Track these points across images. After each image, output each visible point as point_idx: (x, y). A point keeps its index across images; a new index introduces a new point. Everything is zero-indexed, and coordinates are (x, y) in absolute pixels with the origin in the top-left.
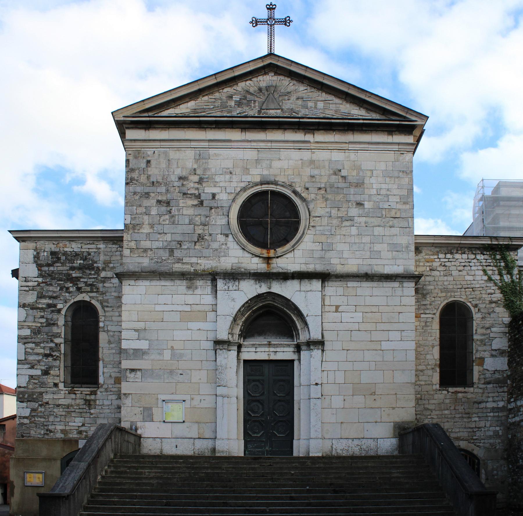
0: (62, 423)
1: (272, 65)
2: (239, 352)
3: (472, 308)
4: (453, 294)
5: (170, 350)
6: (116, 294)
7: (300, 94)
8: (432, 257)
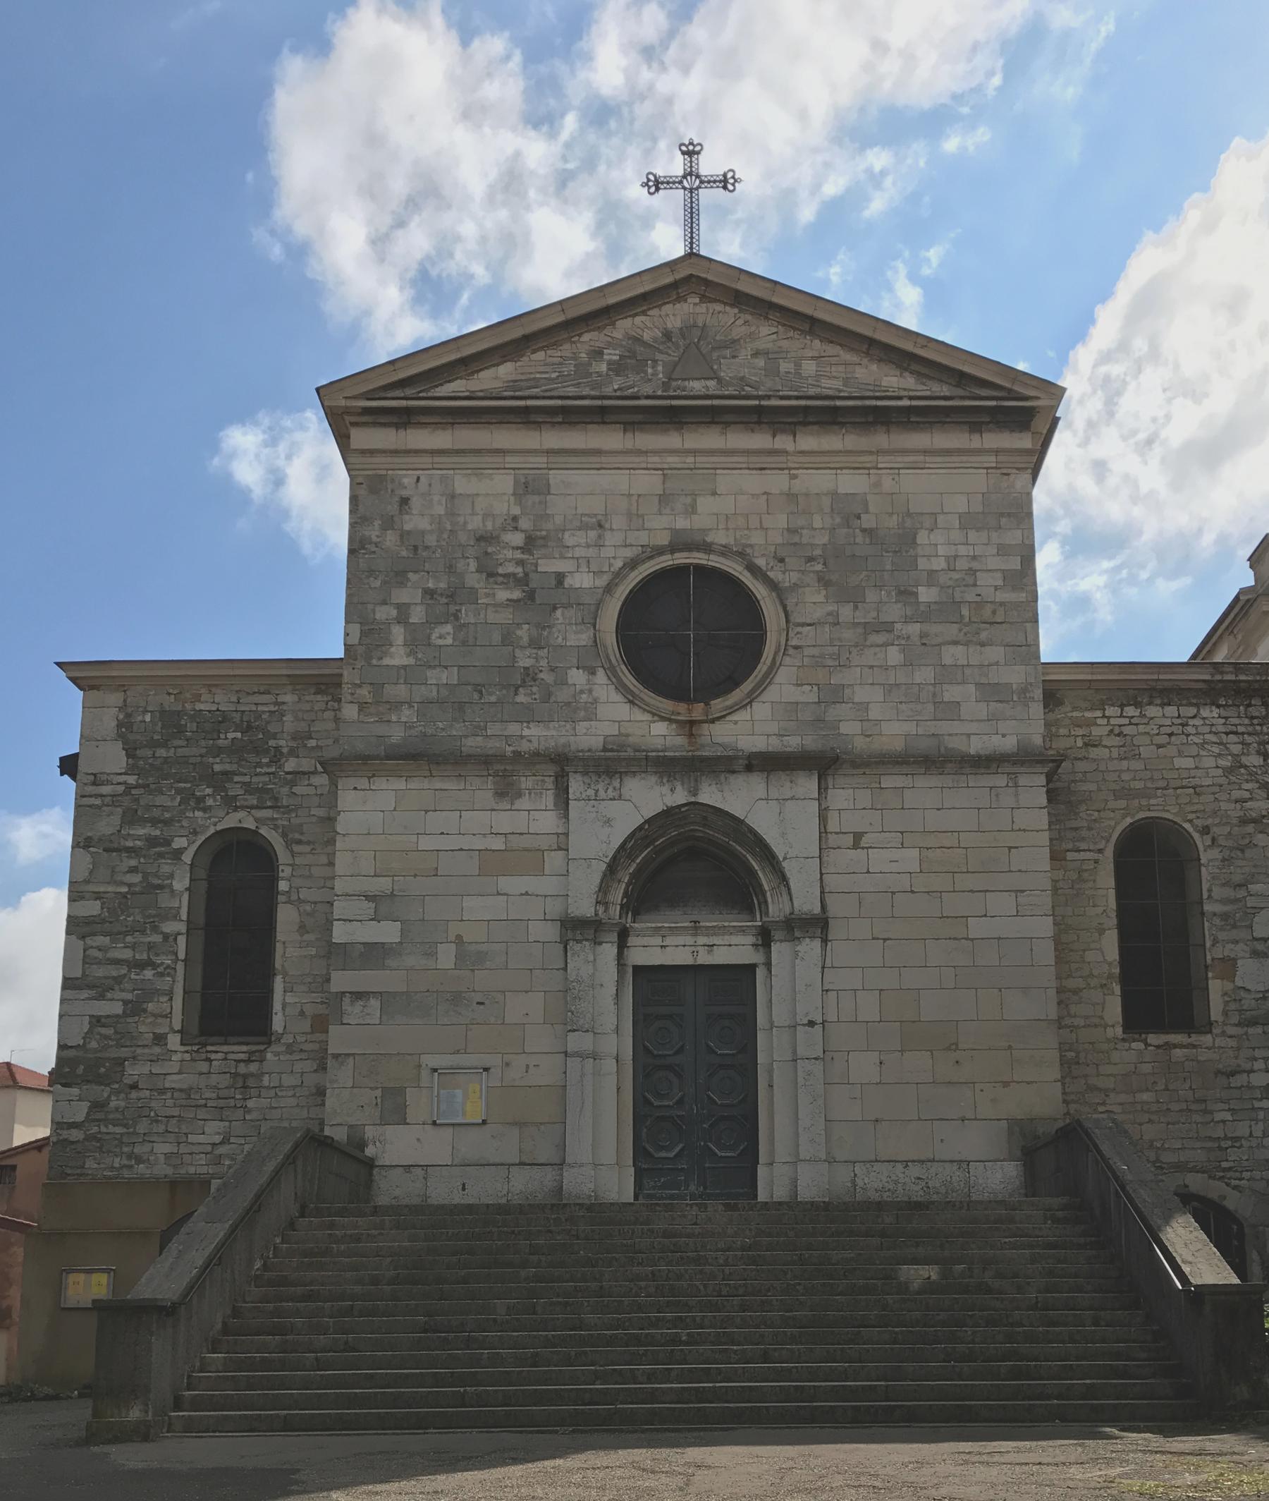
0: (171, 1138)
1: (693, 278)
2: (622, 945)
3: (1196, 836)
4: (1144, 802)
5: (453, 946)
6: (321, 812)
7: (761, 345)
8: (1088, 714)
